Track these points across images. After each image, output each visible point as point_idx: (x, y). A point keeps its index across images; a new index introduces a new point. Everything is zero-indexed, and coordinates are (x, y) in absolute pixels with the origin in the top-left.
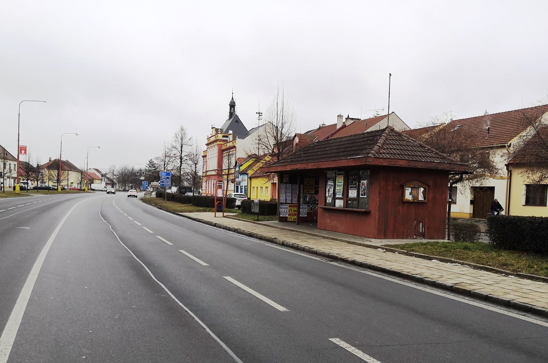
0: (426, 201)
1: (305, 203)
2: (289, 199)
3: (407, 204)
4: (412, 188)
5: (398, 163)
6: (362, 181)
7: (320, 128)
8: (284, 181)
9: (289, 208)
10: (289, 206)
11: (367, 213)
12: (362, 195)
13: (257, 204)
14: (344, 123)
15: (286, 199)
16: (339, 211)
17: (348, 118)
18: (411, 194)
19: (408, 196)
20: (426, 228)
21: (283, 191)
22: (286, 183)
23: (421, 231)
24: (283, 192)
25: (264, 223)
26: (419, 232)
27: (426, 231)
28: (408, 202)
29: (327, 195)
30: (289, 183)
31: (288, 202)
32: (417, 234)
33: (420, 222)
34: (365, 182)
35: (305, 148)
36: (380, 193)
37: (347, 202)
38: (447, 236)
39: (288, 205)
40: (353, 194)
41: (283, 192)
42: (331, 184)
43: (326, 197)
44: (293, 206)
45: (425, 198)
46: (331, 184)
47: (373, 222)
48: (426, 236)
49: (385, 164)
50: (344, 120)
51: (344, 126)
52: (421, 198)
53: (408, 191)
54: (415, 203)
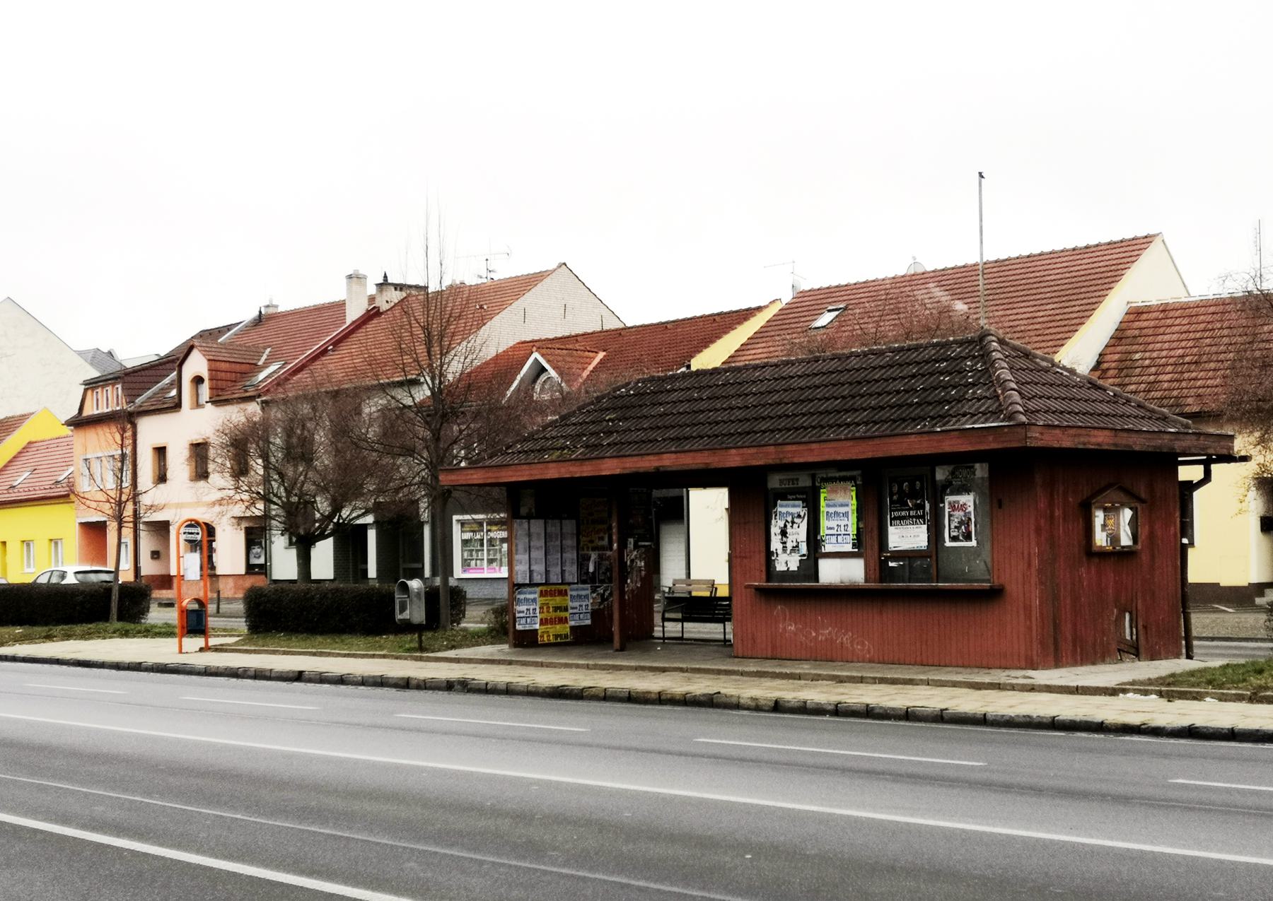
0: (1139, 547)
1: (585, 577)
2: (539, 568)
3: (1096, 560)
4: (1105, 510)
5: (1093, 440)
6: (950, 498)
7: (260, 320)
8: (524, 511)
9: (540, 600)
10: (542, 594)
11: (993, 595)
12: (954, 539)
13: (418, 594)
14: (372, 299)
15: (531, 572)
16: (842, 594)
17: (384, 285)
18: (1104, 526)
19: (1101, 539)
20: (1140, 627)
21: (522, 543)
22: (529, 517)
23: (1128, 638)
24: (521, 547)
25: (451, 654)
26: (1122, 640)
27: (1142, 638)
28: (1103, 555)
29: (776, 544)
30: (538, 516)
31: (538, 578)
32: (1122, 647)
33: (1124, 612)
34: (968, 500)
35: (599, 399)
36: (1038, 530)
37: (883, 564)
38: (1184, 651)
39: (538, 589)
40: (907, 537)
41: (521, 547)
42: (795, 510)
43: (769, 554)
44: (552, 594)
45: (1135, 538)
46: (795, 510)
47: (1013, 622)
48: (1142, 650)
49: (1067, 443)
50: (372, 290)
51: (373, 314)
52: (1126, 540)
53: (1099, 518)
54: (1119, 555)
